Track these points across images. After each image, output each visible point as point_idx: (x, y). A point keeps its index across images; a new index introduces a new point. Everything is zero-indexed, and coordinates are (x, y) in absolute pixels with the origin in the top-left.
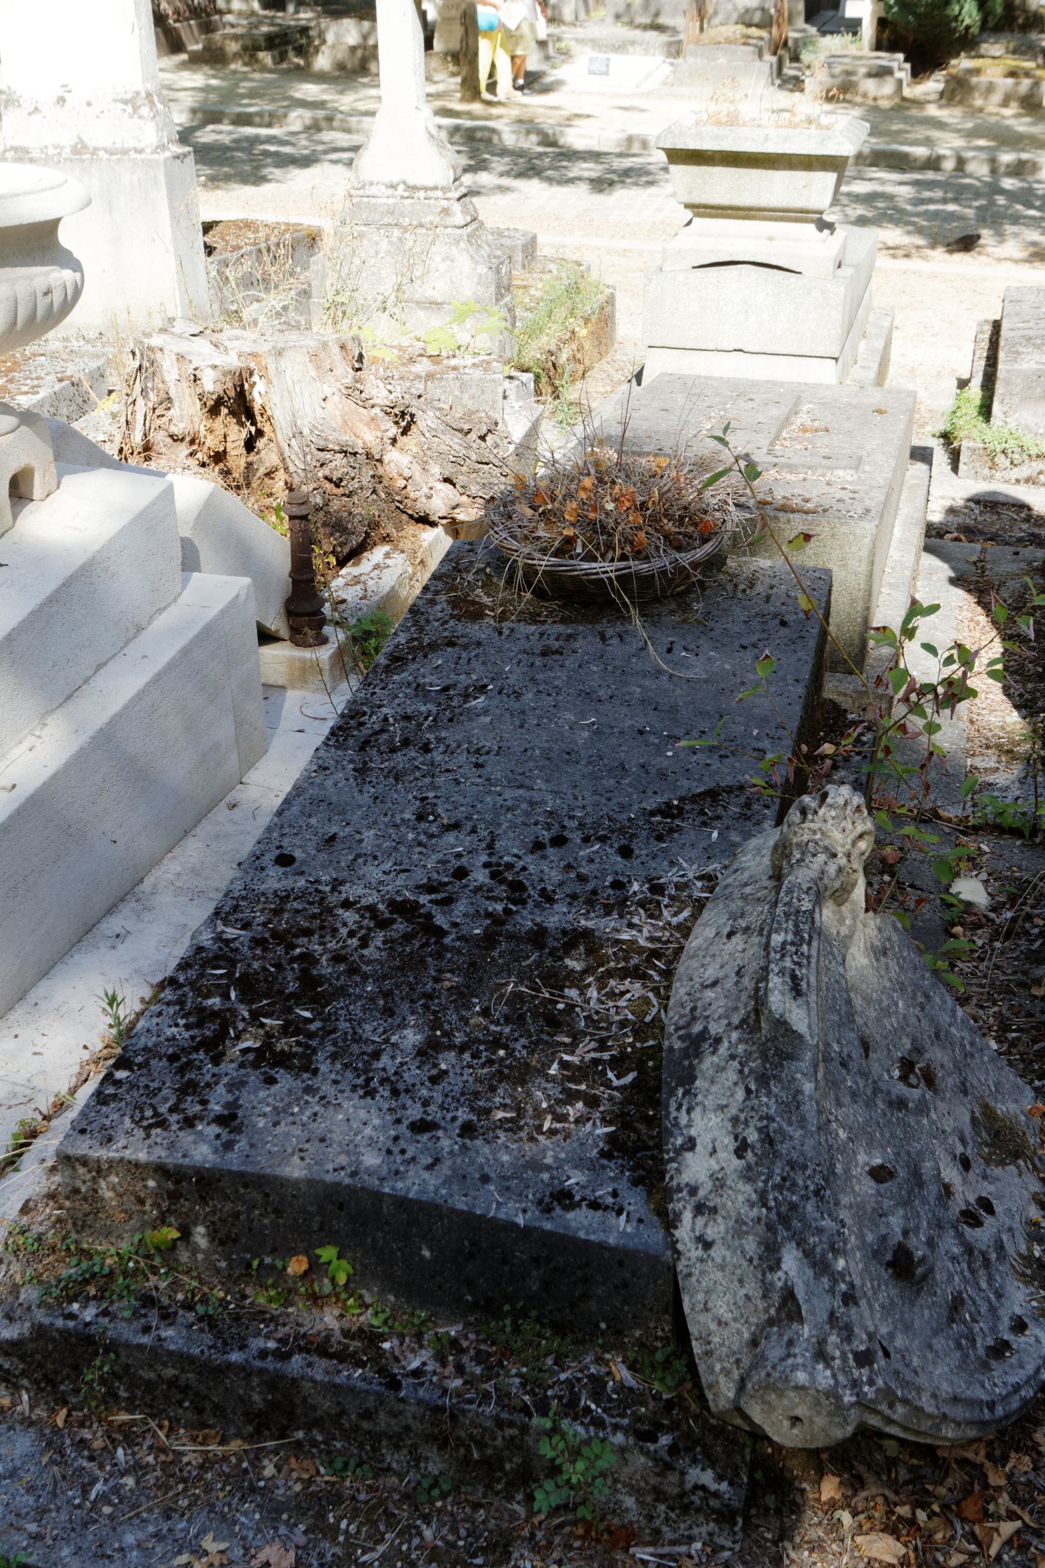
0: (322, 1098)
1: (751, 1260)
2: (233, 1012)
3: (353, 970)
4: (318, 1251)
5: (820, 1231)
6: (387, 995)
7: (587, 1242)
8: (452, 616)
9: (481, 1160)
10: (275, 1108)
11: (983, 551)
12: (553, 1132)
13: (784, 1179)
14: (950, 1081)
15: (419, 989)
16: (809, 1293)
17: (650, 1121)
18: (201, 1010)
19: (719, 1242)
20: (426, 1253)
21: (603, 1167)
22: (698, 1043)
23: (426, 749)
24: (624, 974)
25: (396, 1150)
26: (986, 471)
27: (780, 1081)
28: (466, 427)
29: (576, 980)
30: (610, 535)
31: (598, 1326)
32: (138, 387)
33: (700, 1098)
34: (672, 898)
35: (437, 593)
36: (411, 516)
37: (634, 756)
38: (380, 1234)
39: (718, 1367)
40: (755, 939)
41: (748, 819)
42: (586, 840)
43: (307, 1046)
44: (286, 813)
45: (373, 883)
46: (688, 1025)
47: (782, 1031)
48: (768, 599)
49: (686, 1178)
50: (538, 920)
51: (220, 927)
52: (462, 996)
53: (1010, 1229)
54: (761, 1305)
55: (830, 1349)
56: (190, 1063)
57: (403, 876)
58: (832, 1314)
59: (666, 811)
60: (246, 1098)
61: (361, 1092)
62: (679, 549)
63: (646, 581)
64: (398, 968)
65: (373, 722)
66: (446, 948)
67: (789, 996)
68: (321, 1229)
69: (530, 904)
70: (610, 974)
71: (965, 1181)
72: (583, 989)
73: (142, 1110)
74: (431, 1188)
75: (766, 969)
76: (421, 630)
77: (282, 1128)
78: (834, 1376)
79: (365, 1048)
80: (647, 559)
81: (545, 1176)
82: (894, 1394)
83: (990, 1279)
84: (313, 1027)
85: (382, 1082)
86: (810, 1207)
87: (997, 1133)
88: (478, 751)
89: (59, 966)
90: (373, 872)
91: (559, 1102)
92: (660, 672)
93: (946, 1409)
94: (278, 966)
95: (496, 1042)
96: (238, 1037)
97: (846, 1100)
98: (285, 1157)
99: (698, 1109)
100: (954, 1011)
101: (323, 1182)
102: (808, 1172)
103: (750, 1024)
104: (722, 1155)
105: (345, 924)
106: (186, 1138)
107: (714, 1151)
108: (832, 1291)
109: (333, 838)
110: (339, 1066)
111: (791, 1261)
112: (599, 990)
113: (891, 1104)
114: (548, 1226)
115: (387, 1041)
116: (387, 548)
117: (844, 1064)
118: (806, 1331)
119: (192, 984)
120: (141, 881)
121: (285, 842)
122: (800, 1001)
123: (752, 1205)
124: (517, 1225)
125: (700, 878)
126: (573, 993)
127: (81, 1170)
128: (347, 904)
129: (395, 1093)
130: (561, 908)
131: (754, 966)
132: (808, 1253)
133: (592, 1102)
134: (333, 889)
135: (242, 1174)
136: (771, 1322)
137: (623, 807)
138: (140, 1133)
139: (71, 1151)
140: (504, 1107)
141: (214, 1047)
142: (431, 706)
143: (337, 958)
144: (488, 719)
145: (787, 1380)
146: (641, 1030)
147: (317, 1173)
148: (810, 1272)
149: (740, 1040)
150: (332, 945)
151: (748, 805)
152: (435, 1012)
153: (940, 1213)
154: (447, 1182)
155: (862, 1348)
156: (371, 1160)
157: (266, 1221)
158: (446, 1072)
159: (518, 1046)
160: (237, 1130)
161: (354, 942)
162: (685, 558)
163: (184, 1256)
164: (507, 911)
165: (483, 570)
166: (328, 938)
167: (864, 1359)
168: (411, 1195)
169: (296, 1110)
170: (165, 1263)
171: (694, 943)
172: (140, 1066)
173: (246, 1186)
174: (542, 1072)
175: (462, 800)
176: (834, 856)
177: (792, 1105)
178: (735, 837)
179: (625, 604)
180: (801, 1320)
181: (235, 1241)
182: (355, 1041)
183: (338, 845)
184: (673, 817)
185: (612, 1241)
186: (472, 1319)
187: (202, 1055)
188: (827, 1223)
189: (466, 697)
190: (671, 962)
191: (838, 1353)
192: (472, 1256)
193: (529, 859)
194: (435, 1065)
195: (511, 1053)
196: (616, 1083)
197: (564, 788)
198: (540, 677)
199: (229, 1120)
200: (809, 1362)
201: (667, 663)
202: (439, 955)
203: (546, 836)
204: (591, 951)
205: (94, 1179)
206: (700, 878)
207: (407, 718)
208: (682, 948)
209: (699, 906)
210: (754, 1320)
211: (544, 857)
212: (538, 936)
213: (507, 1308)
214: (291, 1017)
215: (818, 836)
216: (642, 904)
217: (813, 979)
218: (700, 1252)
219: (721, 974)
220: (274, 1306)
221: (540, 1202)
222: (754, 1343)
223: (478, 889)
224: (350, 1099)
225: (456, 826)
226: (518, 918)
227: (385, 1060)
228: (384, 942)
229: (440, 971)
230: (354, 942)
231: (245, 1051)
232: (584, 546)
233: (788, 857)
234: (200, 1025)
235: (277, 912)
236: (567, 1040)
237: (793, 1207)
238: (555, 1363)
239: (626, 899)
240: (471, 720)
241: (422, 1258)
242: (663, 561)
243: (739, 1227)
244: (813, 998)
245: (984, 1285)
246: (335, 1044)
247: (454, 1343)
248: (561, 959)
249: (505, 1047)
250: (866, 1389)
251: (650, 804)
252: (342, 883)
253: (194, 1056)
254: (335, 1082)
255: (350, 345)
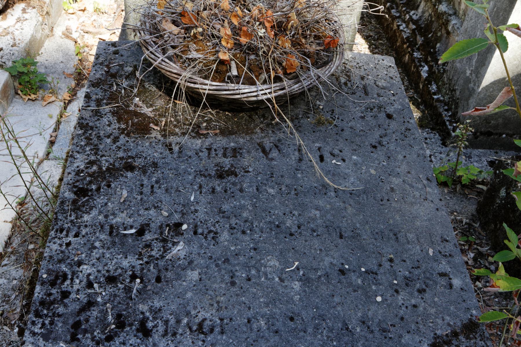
35: (99, 103)
76: (96, 150)
201: (333, 182)
207: (111, 280)
240: (179, 277)
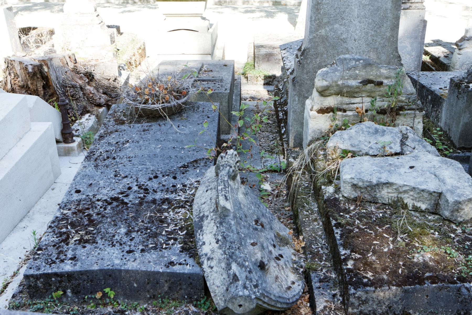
0: (100, 249)
1: (224, 269)
2: (70, 232)
3: (103, 216)
4: (104, 290)
5: (240, 257)
6: (114, 221)
7: (179, 273)
8: (116, 124)
9: (147, 257)
10: (87, 253)
11: (257, 103)
12: (166, 248)
13: (230, 247)
14: (268, 226)
15: (123, 218)
16: (240, 273)
17: (191, 242)
18: (60, 232)
19: (215, 266)
20: (135, 285)
21: (181, 255)
22: (202, 219)
23: (114, 158)
24: (179, 207)
25: (123, 258)
26: (255, 82)
27: (225, 223)
28: (109, 78)
29: (167, 211)
30: (158, 97)
31: (184, 297)
32: (7, 72)
33: (205, 231)
34: (189, 188)
36: (95, 105)
37: (173, 154)
38: (122, 282)
39: (218, 298)
40: (214, 190)
41: (206, 166)
42: (163, 176)
43: (94, 237)
44: (76, 180)
45: (106, 193)
46: (199, 214)
47: (224, 209)
48: (203, 112)
49: (204, 252)
50: (153, 197)
51: (62, 211)
52: (135, 219)
53: (288, 261)
54: (228, 280)
55: (247, 285)
56: (59, 246)
57: (113, 191)
58: (246, 277)
59: (184, 166)
60: (78, 252)
61: (111, 246)
62: (178, 99)
63: (170, 108)
64: (116, 214)
65: (98, 154)
66: (129, 207)
67: (225, 201)
68: (105, 284)
69: (150, 193)
70: (175, 208)
71: (275, 250)
72: (168, 213)
73: (47, 260)
74: (135, 266)
75: (218, 196)
76: (107, 128)
77: (90, 258)
78: (249, 292)
79: (110, 235)
80: (169, 102)
81: (166, 259)
82: (264, 295)
83: (284, 272)
84: (94, 232)
85: (117, 242)
86: (237, 252)
87: (281, 239)
88: (129, 157)
89: (7, 237)
90: (105, 191)
91: (167, 241)
92: (177, 132)
93: (278, 299)
94: (81, 218)
95: (147, 229)
96: (73, 238)
97: (243, 228)
98: (92, 265)
99: (205, 234)
100: (266, 210)
101: (104, 269)
102: (236, 243)
103: (215, 211)
104: (212, 244)
105: (99, 205)
106: (62, 265)
107: (210, 244)
108: (246, 271)
109: (91, 184)
110: (103, 240)
111: (234, 267)
112: (173, 212)
113: (254, 229)
114: (168, 271)
115: (116, 232)
116: (89, 114)
117: (241, 219)
118: (240, 282)
119: (56, 226)
120: (29, 212)
121: (77, 187)
122: (228, 201)
123: (222, 255)
124: (160, 272)
125: (196, 182)
126: (166, 214)
127: (31, 279)
128: (98, 200)
129: (121, 244)
130: (159, 193)
131: (215, 196)
132: (238, 264)
133: (175, 239)
134: (94, 197)
135: (80, 271)
136: (231, 283)
137: (172, 167)
138: (48, 266)
139: (28, 274)
140: (152, 244)
141: (66, 241)
142: (113, 148)
143: (98, 214)
144: (131, 149)
145: (237, 295)
146: (186, 220)
147: (102, 267)
148: (239, 268)
149: (213, 215)
150: (96, 211)
151: (206, 163)
152: (128, 223)
153: (270, 256)
154: (139, 264)
155: (255, 284)
156: (117, 262)
157: (88, 284)
158: (134, 238)
159: (153, 229)
160: (77, 260)
161: (102, 209)
162: (180, 102)
163: (64, 300)
164: (144, 196)
165: (122, 111)
166: (94, 209)
167: (256, 286)
168: (130, 269)
169: (93, 253)
170: (59, 302)
171: (197, 195)
172: (45, 249)
173: (82, 275)
174: (161, 234)
175: (127, 170)
176: (231, 167)
177: (229, 228)
178: (203, 171)
179: (165, 116)
180: (238, 280)
181: (80, 292)
182: (107, 234)
183: (93, 186)
184: (186, 168)
185: (186, 272)
186: (150, 302)
187: (63, 244)
188: (242, 255)
189: (123, 144)
190: (191, 203)
191: (249, 286)
192: (148, 283)
193: (148, 182)
194: (131, 236)
195: (151, 231)
196: (181, 234)
197: (155, 164)
198: (144, 137)
199: (74, 258)
200: (242, 290)
202: (127, 209)
203: (152, 176)
204: (169, 203)
205: (36, 281)
206: (196, 182)
207: (107, 151)
208: (193, 199)
209: (197, 188)
210: (226, 284)
211: (152, 182)
212: (154, 201)
213: (159, 296)
214: (87, 230)
215: (226, 163)
216: (181, 190)
217: (230, 196)
218: (210, 270)
219: (206, 201)
220: (93, 308)
221: (165, 265)
222: (227, 290)
223: (136, 191)
224: (108, 248)
225: (126, 177)
226: (148, 197)
227: (116, 237)
228: (111, 208)
229: (128, 213)
230: (102, 209)
231: (75, 241)
232: (151, 101)
233: (219, 169)
234: (61, 236)
235: (78, 205)
236: (166, 225)
237: (233, 253)
238: (175, 309)
239: (177, 189)
240: (126, 150)
241: (134, 287)
242: (174, 103)
243: (220, 261)
244: (231, 201)
245: (283, 274)
246: (101, 235)
247: (146, 309)
248: (161, 206)
249: (150, 229)
250: (257, 293)
251: (180, 165)
252: (96, 195)
253: (60, 244)
254: (103, 244)
255: (71, 57)
